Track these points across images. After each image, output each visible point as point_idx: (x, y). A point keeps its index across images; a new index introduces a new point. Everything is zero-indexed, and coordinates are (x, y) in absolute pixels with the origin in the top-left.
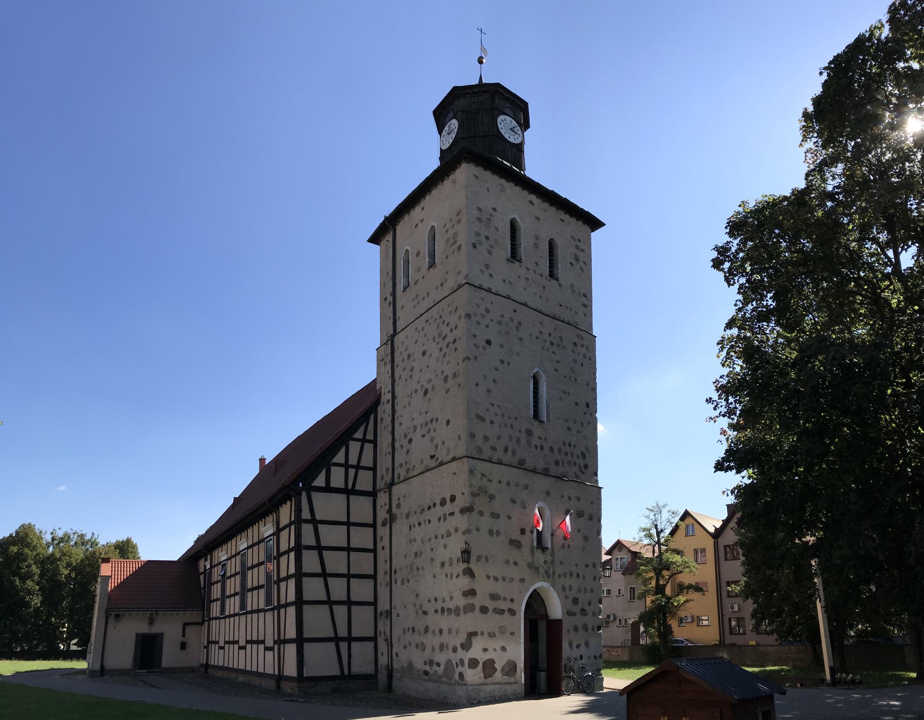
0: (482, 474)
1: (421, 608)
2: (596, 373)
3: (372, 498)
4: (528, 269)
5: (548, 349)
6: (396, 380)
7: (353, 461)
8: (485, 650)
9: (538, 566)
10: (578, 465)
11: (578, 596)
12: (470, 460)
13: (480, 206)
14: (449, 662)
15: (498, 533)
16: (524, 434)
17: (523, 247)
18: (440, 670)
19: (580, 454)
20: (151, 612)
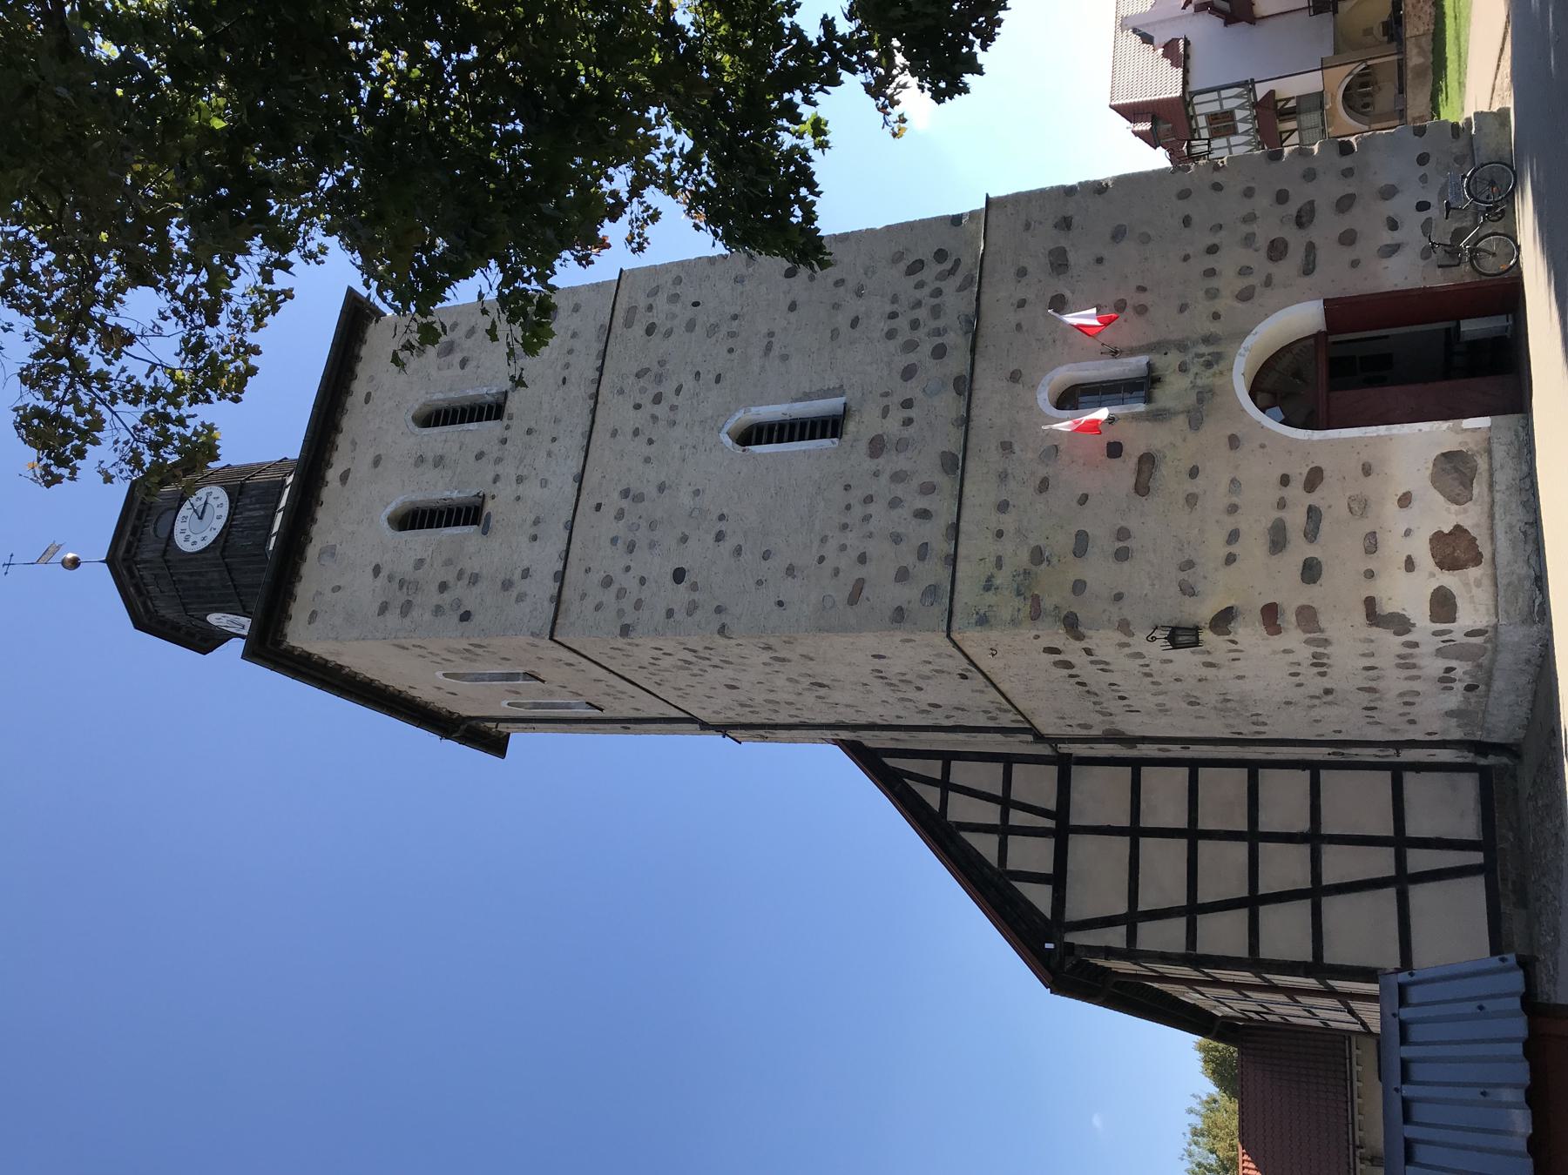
0: (987, 588)
1: (1318, 697)
2: (708, 257)
3: (1074, 768)
4: (496, 479)
6: (801, 722)
7: (990, 814)
8: (1410, 565)
9: (1194, 397)
10: (938, 284)
11: (1262, 242)
12: (955, 626)
13: (376, 608)
14: (1440, 653)
15: (1123, 534)
17: (448, 493)
18: (1461, 668)
20: (1358, 1161)
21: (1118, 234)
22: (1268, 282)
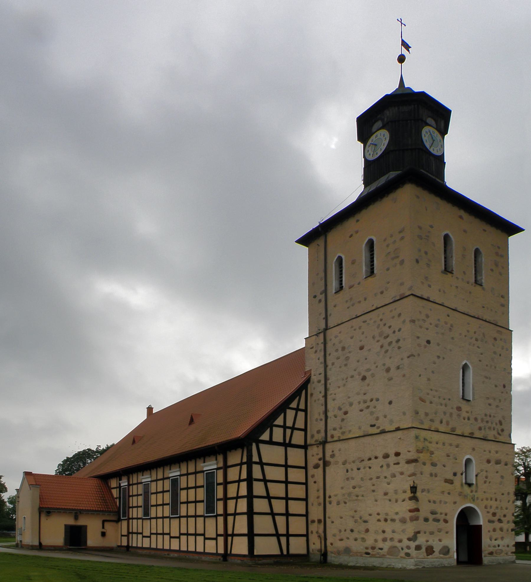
5: (474, 345)
7: (289, 423)
16: (455, 410)
19: (498, 422)
21: (502, 477)
22: (488, 512)
